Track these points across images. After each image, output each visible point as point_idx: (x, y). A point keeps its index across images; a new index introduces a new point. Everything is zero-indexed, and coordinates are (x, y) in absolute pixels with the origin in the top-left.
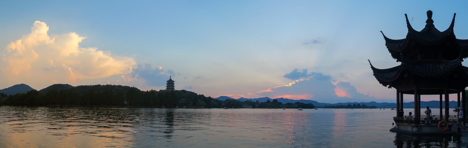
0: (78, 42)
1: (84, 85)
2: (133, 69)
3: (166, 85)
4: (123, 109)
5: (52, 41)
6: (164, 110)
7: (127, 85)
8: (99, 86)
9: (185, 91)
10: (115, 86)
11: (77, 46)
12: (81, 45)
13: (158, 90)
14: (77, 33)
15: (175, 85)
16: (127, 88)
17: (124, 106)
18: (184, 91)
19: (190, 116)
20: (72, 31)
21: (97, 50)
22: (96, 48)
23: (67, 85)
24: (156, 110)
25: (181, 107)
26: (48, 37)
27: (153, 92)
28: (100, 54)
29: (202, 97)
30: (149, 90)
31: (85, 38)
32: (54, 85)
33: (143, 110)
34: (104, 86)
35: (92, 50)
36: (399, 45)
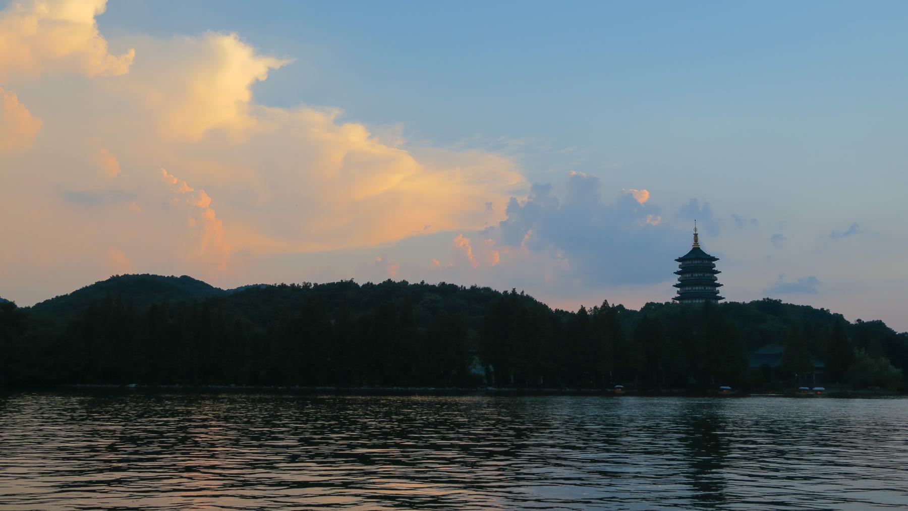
0: (247, 80)
1: (271, 283)
2: (513, 206)
3: (676, 279)
4: (465, 399)
5: (123, 64)
6: (669, 406)
7: (481, 285)
8: (347, 287)
9: (777, 303)
10: (422, 289)
11: (246, 96)
12: (264, 93)
13: (635, 304)
14: (246, 38)
15: (720, 278)
16: (481, 298)
17: (469, 385)
18: (770, 307)
19: (830, 437)
20: (225, 28)
21: (339, 121)
22: (336, 112)
23: (185, 279)
24: (631, 407)
25: (744, 390)
26: (102, 43)
27: (610, 316)
28: (356, 136)
29: (874, 332)
30: (592, 303)
31: (285, 62)
32: (115, 280)
33: (561, 409)
34: (369, 286)
35: (315, 119)
36: (428, 419)
